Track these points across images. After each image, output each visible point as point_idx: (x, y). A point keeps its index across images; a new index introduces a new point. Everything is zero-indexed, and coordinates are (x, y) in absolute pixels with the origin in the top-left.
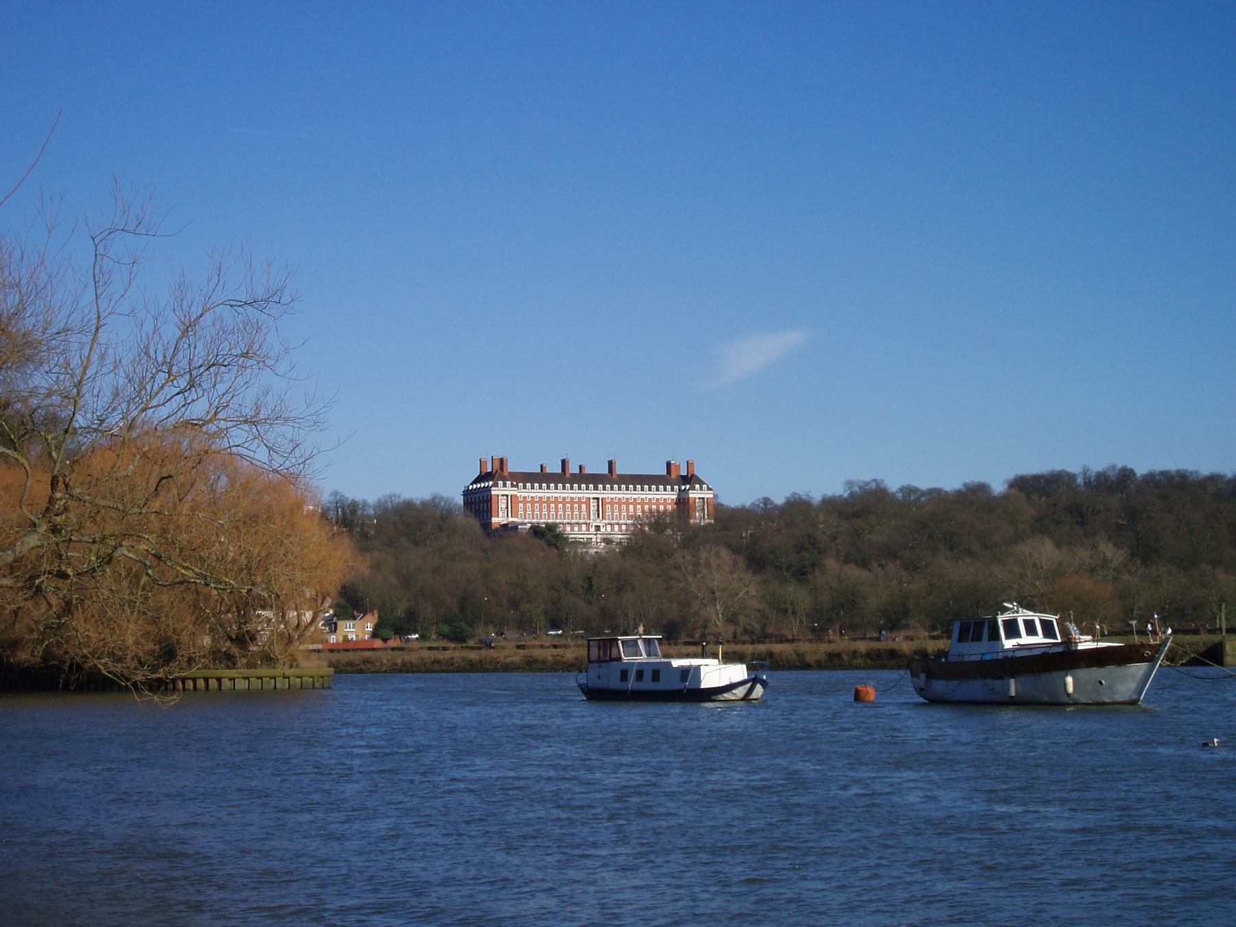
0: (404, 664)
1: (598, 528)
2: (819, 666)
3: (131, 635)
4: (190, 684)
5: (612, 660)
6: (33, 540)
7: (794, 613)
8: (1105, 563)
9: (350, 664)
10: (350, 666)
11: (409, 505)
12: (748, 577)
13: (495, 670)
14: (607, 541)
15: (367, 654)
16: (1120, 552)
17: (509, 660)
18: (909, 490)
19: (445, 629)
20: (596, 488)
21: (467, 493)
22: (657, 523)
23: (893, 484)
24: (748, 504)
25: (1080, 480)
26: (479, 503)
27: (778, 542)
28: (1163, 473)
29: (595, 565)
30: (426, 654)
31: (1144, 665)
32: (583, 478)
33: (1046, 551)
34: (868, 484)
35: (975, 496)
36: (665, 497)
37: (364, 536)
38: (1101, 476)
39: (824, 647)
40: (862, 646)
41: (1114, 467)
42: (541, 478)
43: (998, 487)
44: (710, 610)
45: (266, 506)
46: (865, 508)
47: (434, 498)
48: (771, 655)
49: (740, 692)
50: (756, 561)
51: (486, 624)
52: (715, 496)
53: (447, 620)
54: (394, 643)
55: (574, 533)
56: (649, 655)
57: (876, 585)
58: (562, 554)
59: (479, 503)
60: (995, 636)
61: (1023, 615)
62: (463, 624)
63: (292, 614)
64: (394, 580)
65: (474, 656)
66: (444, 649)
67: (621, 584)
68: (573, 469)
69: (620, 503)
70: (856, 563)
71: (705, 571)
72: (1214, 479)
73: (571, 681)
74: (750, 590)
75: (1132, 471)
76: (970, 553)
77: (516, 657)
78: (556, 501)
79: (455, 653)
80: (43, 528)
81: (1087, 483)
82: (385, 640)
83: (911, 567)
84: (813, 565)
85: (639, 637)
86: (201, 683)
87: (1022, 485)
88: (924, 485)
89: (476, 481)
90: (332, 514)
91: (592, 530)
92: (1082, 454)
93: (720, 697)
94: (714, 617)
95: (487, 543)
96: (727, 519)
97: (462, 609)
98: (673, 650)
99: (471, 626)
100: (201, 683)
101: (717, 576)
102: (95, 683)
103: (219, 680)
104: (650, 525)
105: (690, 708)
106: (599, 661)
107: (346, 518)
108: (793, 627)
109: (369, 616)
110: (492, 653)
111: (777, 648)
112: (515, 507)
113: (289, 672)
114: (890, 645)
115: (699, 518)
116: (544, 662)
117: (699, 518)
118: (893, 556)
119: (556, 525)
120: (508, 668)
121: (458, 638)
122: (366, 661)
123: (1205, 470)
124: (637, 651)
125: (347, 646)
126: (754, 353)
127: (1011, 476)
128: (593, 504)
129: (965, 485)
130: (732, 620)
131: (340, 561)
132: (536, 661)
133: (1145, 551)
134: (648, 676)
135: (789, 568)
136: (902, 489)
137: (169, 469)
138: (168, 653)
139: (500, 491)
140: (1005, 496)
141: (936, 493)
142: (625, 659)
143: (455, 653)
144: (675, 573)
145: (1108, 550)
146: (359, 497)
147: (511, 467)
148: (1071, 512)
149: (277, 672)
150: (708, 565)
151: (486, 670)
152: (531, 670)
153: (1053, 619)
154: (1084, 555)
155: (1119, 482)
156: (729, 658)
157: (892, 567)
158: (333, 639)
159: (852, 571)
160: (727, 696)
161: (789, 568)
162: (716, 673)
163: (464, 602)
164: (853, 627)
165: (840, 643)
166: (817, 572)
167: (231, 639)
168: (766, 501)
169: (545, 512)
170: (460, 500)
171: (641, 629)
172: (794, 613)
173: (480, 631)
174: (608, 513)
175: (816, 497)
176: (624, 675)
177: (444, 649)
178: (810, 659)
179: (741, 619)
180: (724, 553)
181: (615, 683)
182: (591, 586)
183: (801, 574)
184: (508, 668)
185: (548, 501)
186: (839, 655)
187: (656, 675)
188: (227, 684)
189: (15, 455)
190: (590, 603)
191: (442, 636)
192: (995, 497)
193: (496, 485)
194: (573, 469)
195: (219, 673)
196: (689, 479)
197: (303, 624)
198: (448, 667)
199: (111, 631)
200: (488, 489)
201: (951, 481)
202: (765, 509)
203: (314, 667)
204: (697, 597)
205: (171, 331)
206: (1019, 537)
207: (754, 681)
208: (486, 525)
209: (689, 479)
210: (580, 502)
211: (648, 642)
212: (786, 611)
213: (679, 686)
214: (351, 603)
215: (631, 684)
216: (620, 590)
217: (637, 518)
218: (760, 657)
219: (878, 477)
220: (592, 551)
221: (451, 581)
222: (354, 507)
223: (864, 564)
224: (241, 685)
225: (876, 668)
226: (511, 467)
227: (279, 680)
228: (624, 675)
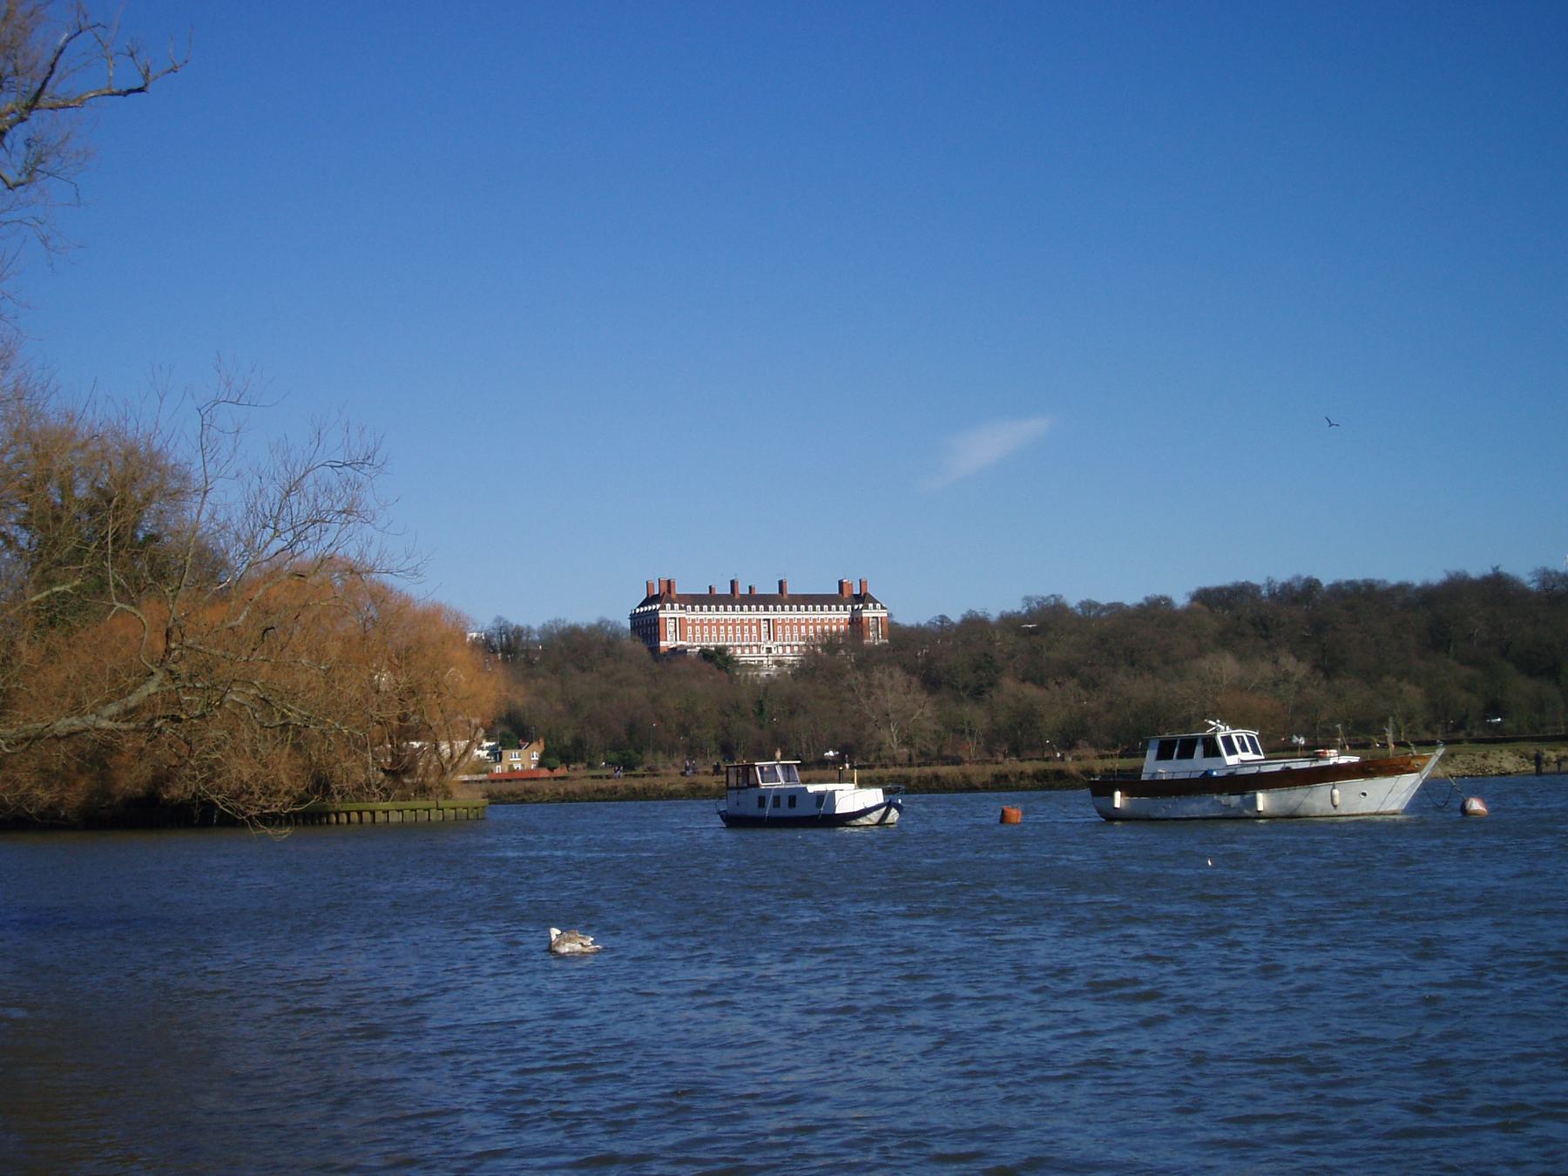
0: (567, 793)
1: (769, 650)
2: (986, 787)
3: (286, 774)
4: (344, 818)
5: (750, 786)
6: (152, 687)
7: (971, 733)
8: (1287, 677)
9: (512, 794)
10: (509, 795)
11: (574, 631)
12: (922, 697)
13: (659, 798)
14: (779, 663)
15: (528, 784)
16: (1302, 665)
17: (672, 788)
18: (1088, 605)
19: (613, 756)
20: (766, 609)
21: (633, 617)
22: (830, 643)
23: (1073, 600)
24: (923, 623)
25: (1264, 592)
26: (646, 626)
27: (954, 660)
28: (1349, 583)
29: (766, 689)
30: (589, 783)
31: (1415, 776)
32: (753, 599)
33: (1227, 666)
34: (1045, 599)
35: (1156, 611)
36: (839, 617)
37: (530, 663)
38: (1287, 588)
39: (991, 769)
40: (1029, 767)
41: (1299, 578)
42: (710, 599)
43: (1181, 600)
44: (884, 732)
45: (413, 640)
46: (1047, 621)
47: (599, 624)
48: (937, 777)
49: (875, 817)
50: (932, 681)
51: (655, 751)
52: (890, 615)
53: (615, 748)
54: (559, 772)
55: (744, 656)
56: (788, 780)
57: (1055, 704)
58: (732, 678)
59: (646, 626)
60: (1216, 753)
61: (1222, 731)
62: (631, 751)
63: (445, 747)
64: (560, 707)
65: (637, 784)
66: (608, 777)
67: (793, 707)
68: (743, 590)
69: (791, 623)
70: (1035, 683)
71: (879, 692)
72: (1402, 588)
73: (711, 806)
74: (923, 710)
75: (1317, 582)
76: (1151, 668)
77: (680, 784)
78: (726, 623)
79: (620, 780)
80: (159, 676)
81: (1273, 595)
82: (552, 769)
83: (1089, 684)
84: (991, 684)
85: (778, 763)
86: (354, 817)
87: (1205, 597)
88: (1104, 600)
89: (642, 605)
90: (495, 641)
91: (764, 652)
92: (1266, 563)
93: (853, 822)
94: (888, 740)
95: (656, 668)
96: (902, 639)
97: (630, 734)
98: (816, 773)
99: (639, 752)
100: (354, 817)
101: (890, 696)
102: (200, 816)
103: (373, 813)
104: (822, 646)
105: (824, 833)
106: (738, 788)
107: (508, 648)
108: (970, 748)
109: (534, 745)
110: (657, 781)
111: (944, 770)
112: (685, 630)
113: (442, 803)
114: (1059, 766)
115: (874, 638)
116: (708, 789)
117: (874, 638)
118: (1073, 673)
119: (725, 648)
120: (671, 796)
121: (628, 766)
122: (528, 791)
123: (1393, 578)
124: (775, 777)
125: (512, 776)
126: (986, 446)
127: (1193, 589)
128: (764, 625)
129: (1146, 599)
130: (907, 742)
131: (491, 689)
132: (700, 787)
133: (1329, 666)
134: (784, 802)
135: (965, 687)
136: (1082, 604)
137: (272, 620)
138: (321, 785)
139: (668, 614)
140: (1188, 611)
141: (1117, 608)
142: (763, 785)
143: (620, 780)
144: (848, 695)
145: (1289, 662)
146: (523, 623)
147: (679, 590)
148: (1254, 625)
149: (432, 804)
150: (881, 686)
151: (649, 799)
152: (695, 797)
153: (1254, 734)
154: (1265, 669)
155: (1304, 594)
156: (863, 783)
157: (1071, 684)
158: (498, 769)
159: (1030, 690)
160: (862, 821)
161: (965, 687)
162: (850, 798)
163: (631, 729)
164: (1032, 747)
165: (1011, 765)
166: (993, 692)
167: (384, 770)
168: (943, 618)
169: (714, 634)
170: (627, 624)
171: (778, 754)
172: (971, 733)
173: (648, 758)
174: (780, 634)
175: (994, 615)
176: (762, 801)
177: (608, 777)
178: (976, 781)
179: (917, 740)
180: (898, 673)
181: (752, 809)
182: (762, 710)
183: (977, 693)
184: (671, 796)
185: (718, 623)
186: (1005, 777)
187: (792, 801)
188: (380, 817)
189: (133, 609)
190: (761, 727)
191: (610, 763)
192: (1176, 612)
193: (663, 608)
194: (743, 590)
195: (372, 806)
196: (862, 598)
197: (457, 754)
198: (612, 796)
199: (253, 765)
200: (656, 612)
201: (1132, 596)
202: (941, 627)
203: (475, 798)
204: (870, 719)
205: (274, 493)
206: (1201, 652)
207: (889, 805)
208: (654, 649)
209: (862, 598)
210: (750, 623)
211: (787, 768)
212: (963, 732)
213: (815, 812)
214: (512, 730)
215: (768, 811)
216: (792, 713)
217: (808, 639)
218: (892, 779)
219: (1057, 593)
220: (763, 674)
221: (615, 705)
222: (518, 632)
223: (1040, 682)
224: (395, 817)
225: (1042, 789)
226: (679, 590)
227: (433, 811)
228: (762, 801)
